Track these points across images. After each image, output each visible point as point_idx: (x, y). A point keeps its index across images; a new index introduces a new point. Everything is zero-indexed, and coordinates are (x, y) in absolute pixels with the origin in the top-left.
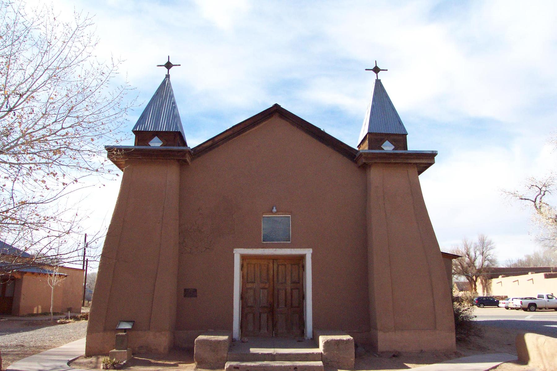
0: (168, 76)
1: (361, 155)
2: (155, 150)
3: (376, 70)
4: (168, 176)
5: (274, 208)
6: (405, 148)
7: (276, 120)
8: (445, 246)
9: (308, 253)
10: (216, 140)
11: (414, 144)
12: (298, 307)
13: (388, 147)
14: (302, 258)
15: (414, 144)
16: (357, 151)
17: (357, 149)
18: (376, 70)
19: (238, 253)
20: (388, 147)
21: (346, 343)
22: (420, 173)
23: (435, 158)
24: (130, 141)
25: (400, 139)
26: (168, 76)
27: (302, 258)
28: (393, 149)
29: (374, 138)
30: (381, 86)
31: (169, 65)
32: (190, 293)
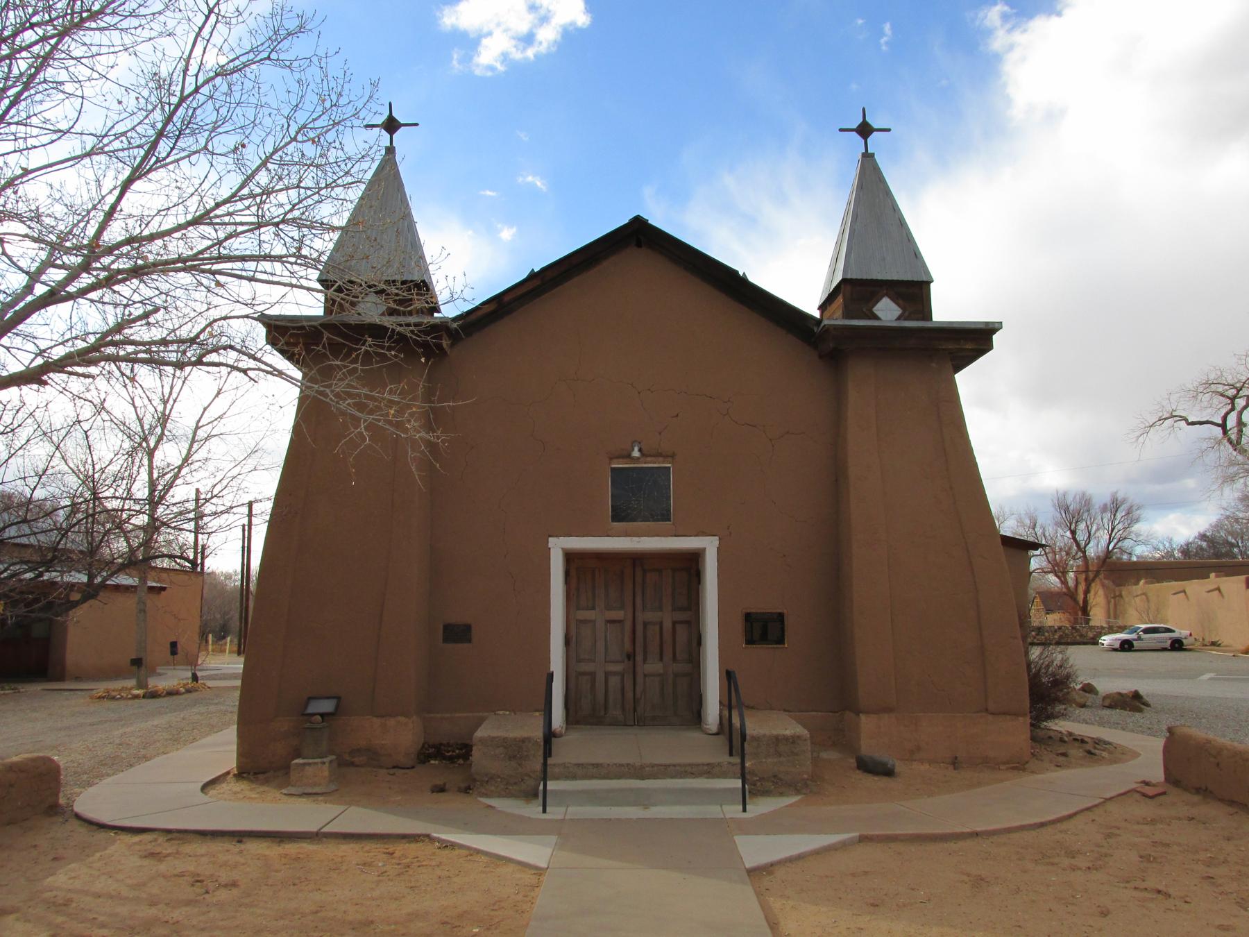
0: (390, 150)
1: (827, 330)
2: (368, 335)
3: (865, 130)
4: (396, 411)
5: (636, 449)
6: (927, 314)
7: (637, 260)
8: (1008, 528)
9: (709, 546)
10: (507, 298)
11: (949, 305)
12: (623, 676)
13: (887, 311)
14: (693, 560)
15: (949, 305)
16: (818, 322)
17: (817, 314)
18: (865, 130)
19: (558, 546)
20: (887, 311)
21: (793, 742)
22: (958, 368)
23: (995, 337)
24: (310, 305)
25: (915, 293)
26: (390, 150)
27: (693, 560)
28: (899, 319)
29: (852, 292)
30: (876, 170)
31: (391, 125)
32: (458, 633)
